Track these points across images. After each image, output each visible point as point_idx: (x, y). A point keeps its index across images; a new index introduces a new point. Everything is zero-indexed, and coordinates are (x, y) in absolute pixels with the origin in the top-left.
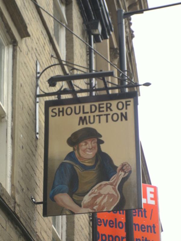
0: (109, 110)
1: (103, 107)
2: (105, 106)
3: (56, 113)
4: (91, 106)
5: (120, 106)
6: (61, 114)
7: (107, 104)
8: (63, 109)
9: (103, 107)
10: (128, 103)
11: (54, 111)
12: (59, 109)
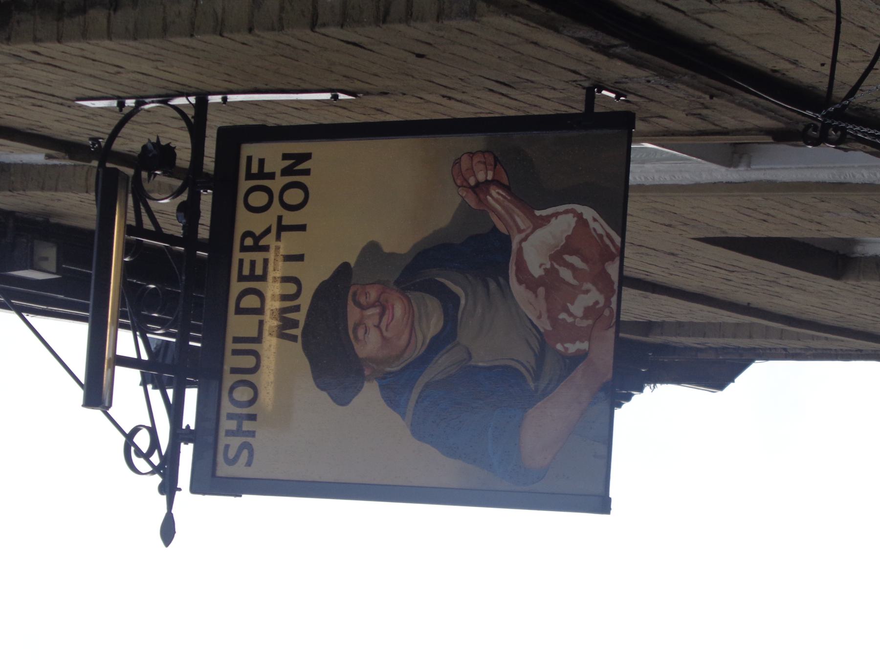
0: (262, 243)
1: (253, 264)
2: (248, 257)
3: (246, 446)
4: (239, 311)
5: (258, 199)
6: (247, 426)
7: (244, 249)
8: (230, 417)
9: (253, 264)
10: (255, 169)
11: (231, 454)
12: (229, 433)
